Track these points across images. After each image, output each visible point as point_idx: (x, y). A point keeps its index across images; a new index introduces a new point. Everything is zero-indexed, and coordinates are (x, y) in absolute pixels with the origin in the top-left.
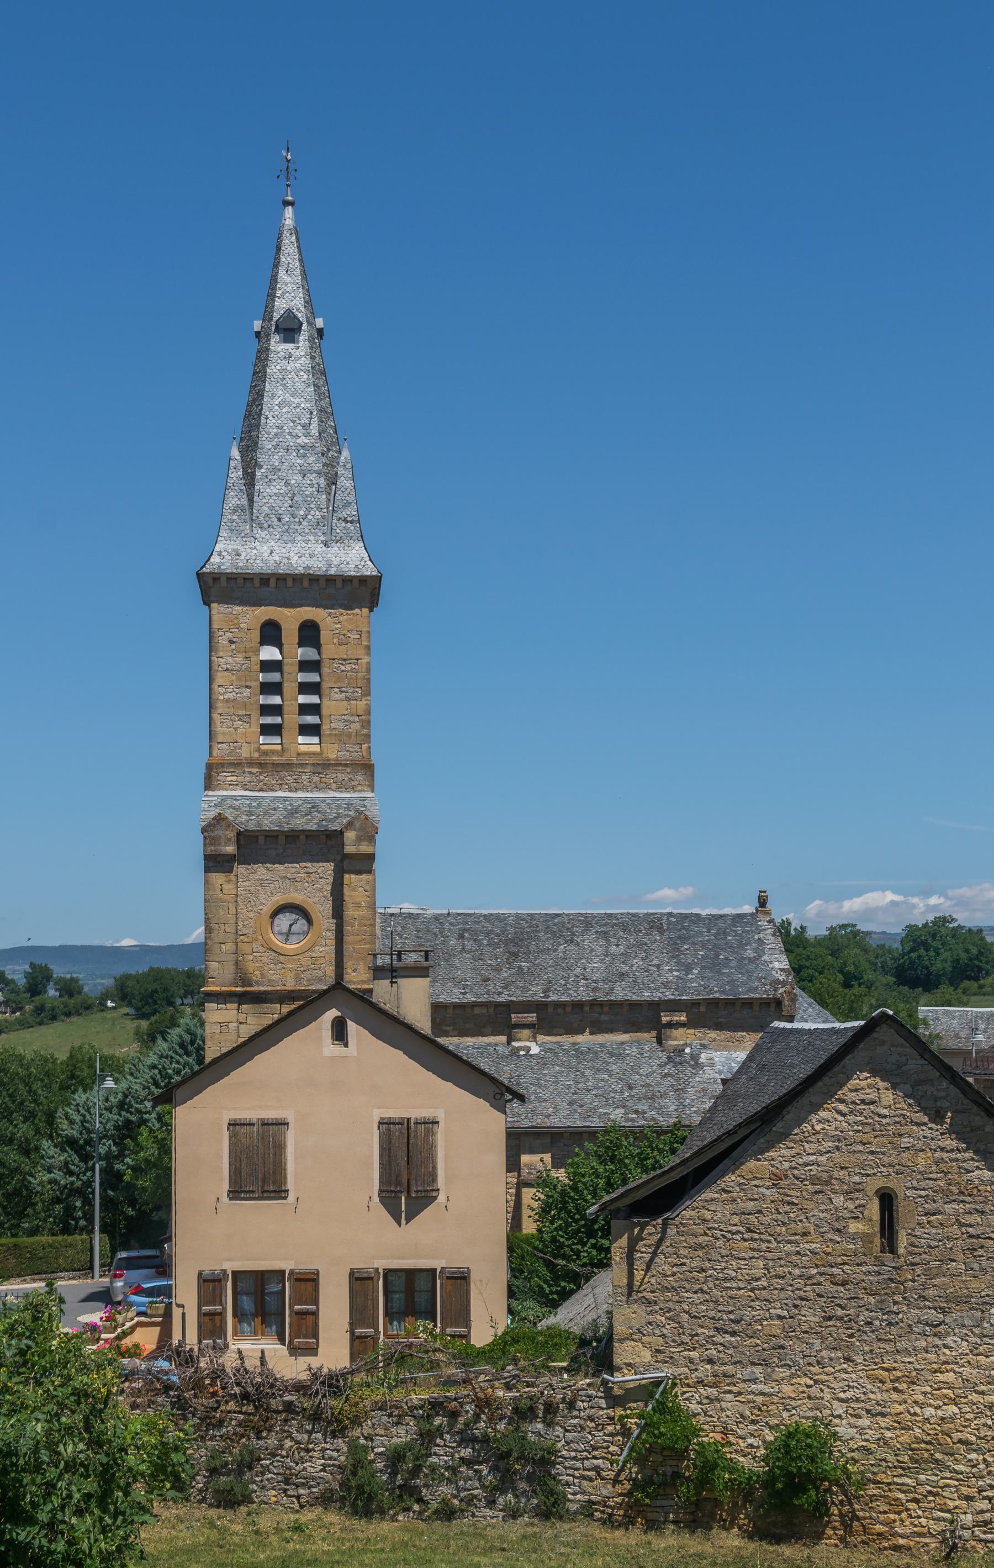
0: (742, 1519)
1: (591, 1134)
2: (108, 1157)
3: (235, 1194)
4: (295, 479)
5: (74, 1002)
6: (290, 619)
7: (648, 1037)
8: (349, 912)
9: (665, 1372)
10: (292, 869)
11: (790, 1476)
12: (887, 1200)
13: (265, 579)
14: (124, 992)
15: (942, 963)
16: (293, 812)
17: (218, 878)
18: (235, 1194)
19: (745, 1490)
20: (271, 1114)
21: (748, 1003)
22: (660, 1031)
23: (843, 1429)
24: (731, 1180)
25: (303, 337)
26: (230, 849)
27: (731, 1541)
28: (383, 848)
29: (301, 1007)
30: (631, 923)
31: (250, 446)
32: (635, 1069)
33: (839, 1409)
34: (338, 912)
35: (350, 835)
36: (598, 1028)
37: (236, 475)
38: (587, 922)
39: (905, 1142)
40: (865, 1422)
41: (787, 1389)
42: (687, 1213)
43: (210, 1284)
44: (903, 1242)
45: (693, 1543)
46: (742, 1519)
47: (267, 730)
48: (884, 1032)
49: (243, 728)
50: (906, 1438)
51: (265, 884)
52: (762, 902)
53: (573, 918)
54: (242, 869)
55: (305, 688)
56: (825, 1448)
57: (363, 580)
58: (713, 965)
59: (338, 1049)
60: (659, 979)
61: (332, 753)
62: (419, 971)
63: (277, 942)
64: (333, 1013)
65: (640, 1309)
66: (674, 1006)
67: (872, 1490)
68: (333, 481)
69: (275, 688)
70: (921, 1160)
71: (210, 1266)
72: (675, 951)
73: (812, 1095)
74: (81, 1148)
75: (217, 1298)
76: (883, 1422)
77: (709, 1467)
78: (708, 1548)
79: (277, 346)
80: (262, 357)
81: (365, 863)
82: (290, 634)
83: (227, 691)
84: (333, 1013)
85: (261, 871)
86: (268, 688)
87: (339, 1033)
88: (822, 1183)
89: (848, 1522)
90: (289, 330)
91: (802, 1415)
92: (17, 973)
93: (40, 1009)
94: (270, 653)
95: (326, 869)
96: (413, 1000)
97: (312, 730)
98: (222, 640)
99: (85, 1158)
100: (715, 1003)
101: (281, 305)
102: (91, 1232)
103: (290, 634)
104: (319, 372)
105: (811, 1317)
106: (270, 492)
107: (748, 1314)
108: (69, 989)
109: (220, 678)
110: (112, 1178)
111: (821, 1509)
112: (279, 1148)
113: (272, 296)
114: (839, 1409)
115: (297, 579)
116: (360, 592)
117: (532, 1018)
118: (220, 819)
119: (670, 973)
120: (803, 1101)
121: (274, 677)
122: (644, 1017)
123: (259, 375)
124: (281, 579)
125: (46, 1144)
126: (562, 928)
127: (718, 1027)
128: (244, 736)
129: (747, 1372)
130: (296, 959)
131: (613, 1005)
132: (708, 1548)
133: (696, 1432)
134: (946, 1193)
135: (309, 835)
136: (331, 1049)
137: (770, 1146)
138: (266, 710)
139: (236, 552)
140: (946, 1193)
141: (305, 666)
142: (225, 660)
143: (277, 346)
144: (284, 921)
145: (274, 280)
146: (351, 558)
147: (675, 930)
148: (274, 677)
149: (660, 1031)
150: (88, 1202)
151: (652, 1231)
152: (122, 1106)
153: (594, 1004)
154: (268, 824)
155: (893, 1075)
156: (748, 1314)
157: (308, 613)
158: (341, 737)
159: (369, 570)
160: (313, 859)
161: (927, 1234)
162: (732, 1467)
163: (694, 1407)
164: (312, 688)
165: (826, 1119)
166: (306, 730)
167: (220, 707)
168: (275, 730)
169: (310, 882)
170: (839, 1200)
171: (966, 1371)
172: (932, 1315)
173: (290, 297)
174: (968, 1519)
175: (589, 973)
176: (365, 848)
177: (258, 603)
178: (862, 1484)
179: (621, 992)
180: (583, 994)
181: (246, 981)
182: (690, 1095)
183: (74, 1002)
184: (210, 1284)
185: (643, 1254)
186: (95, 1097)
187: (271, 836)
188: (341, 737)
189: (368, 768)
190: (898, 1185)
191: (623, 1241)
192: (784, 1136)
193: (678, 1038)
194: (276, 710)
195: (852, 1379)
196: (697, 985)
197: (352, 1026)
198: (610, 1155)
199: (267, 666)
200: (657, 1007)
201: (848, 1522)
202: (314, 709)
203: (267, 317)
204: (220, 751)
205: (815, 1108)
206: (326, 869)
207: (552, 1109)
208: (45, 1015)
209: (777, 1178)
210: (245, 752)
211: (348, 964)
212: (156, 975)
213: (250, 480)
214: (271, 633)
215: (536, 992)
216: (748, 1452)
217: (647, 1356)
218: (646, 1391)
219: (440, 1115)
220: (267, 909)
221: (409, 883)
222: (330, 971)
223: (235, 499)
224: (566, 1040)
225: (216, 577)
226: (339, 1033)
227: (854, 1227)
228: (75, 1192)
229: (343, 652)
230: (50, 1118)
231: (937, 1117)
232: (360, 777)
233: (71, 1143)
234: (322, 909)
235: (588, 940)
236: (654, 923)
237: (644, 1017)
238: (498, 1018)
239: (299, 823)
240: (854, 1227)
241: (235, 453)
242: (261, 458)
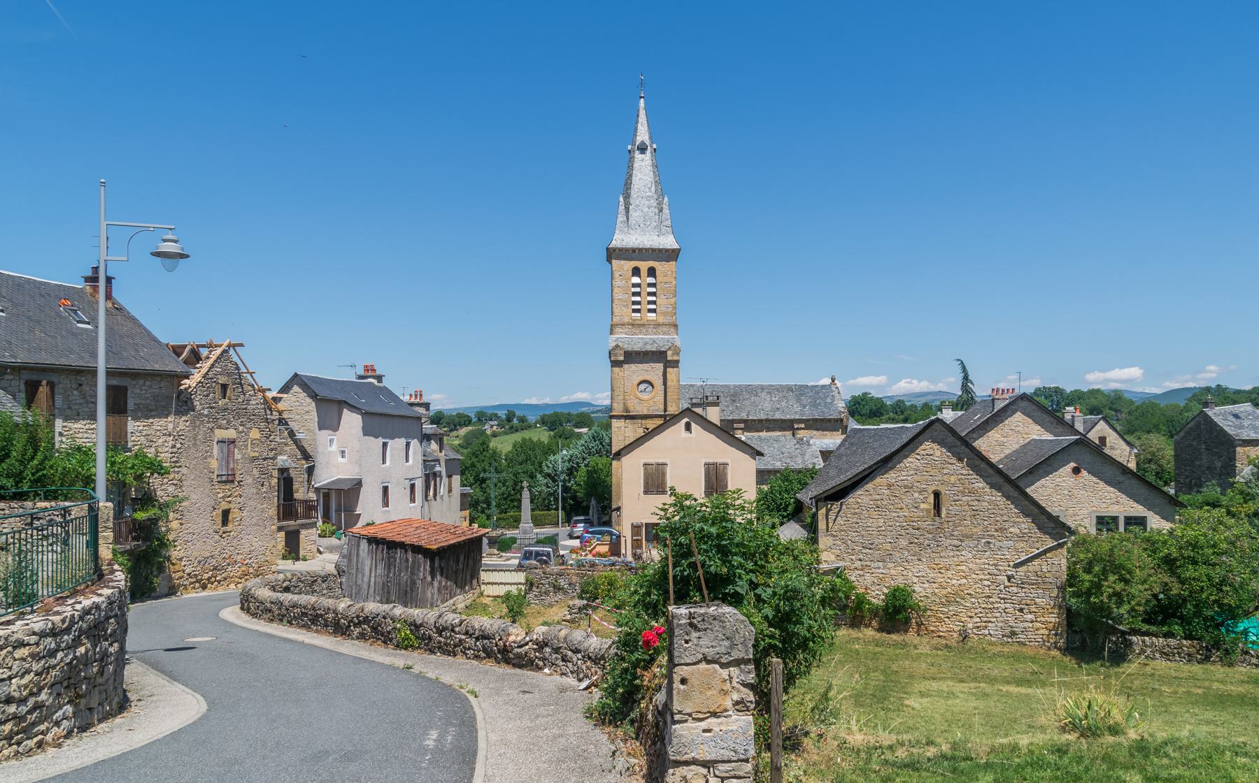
0: (874, 623)
1: (776, 472)
2: (564, 481)
3: (646, 492)
4: (646, 209)
5: (524, 425)
6: (644, 266)
7: (789, 433)
8: (669, 383)
9: (841, 564)
10: (645, 366)
11: (895, 606)
12: (937, 495)
13: (634, 250)
14: (543, 421)
15: (865, 410)
16: (646, 343)
17: (617, 370)
18: (646, 492)
19: (875, 612)
20: (661, 461)
21: (830, 420)
22: (794, 432)
23: (917, 588)
24: (869, 486)
25: (648, 152)
26: (622, 358)
27: (869, 633)
28: (682, 358)
29: (668, 420)
30: (780, 389)
31: (627, 197)
32: (784, 446)
33: (915, 580)
34: (665, 383)
35: (669, 353)
36: (768, 430)
37: (622, 208)
38: (762, 388)
39: (945, 471)
40: (926, 585)
41: (893, 572)
42: (850, 500)
43: (636, 529)
44: (944, 512)
45: (854, 633)
46: (874, 623)
47: (635, 311)
48: (937, 426)
49: (625, 310)
50: (944, 592)
51: (636, 372)
52: (833, 380)
53: (756, 387)
54: (626, 366)
55: (650, 294)
56: (909, 595)
57: (673, 250)
58: (814, 405)
59: (687, 435)
60: (793, 410)
61: (661, 320)
62: (716, 404)
63: (639, 395)
64: (686, 420)
65: (830, 539)
66: (799, 421)
67: (929, 613)
68: (661, 210)
69: (638, 294)
70: (953, 479)
71: (637, 521)
72: (799, 400)
73: (905, 452)
74: (553, 478)
75: (639, 534)
76: (935, 585)
77: (861, 601)
78: (860, 635)
79: (638, 155)
80: (631, 160)
81: (675, 364)
82: (644, 272)
83: (618, 295)
84: (686, 420)
85: (633, 367)
86: (635, 294)
87: (688, 427)
88: (909, 488)
89: (919, 625)
90: (642, 149)
91: (900, 582)
92: (502, 414)
93: (512, 427)
94: (636, 280)
95: (660, 366)
96: (714, 415)
97: (654, 311)
98: (617, 275)
99: (554, 481)
100: (816, 420)
101: (639, 139)
102: (557, 509)
103: (644, 272)
104: (655, 166)
105: (904, 543)
106: (635, 214)
107: (877, 541)
108: (522, 420)
109: (616, 290)
110: (566, 489)
111: (907, 621)
112: (664, 474)
113: (635, 135)
114: (915, 580)
115: (647, 250)
116: (670, 255)
117: (742, 426)
118: (617, 346)
119: (797, 408)
120: (901, 454)
121: (638, 290)
122: (787, 425)
123: (630, 167)
124: (641, 250)
125: (539, 476)
126: (753, 390)
127: (817, 430)
128: (624, 313)
129: (876, 565)
130: (649, 401)
131: (775, 420)
132: (860, 635)
133: (854, 588)
134: (963, 492)
135: (653, 352)
136: (685, 434)
137: (886, 472)
138: (634, 303)
139: (623, 239)
140: (963, 492)
141: (650, 285)
142: (617, 283)
143: (638, 155)
144: (643, 387)
145: (636, 129)
146: (669, 242)
147: (799, 391)
148: (638, 290)
149: (794, 432)
150: (556, 500)
151: (836, 506)
152: (569, 461)
153: (767, 420)
154: (636, 348)
155: (942, 443)
156: (877, 541)
157: (651, 264)
158: (665, 314)
159: (676, 246)
160: (654, 362)
161: (954, 510)
162: (869, 603)
163: (853, 578)
164: (654, 294)
165: (911, 462)
166: (650, 311)
167: (616, 302)
168: (638, 311)
169: (653, 371)
170: (916, 495)
171: (971, 565)
172: (956, 542)
173: (643, 135)
174: (970, 626)
175: (764, 408)
176: (675, 358)
177: (631, 260)
178: (925, 610)
179: (778, 416)
180: (763, 417)
181: (627, 411)
182: (807, 457)
183: (524, 425)
184: (636, 529)
185: (832, 516)
186: (558, 457)
187: (638, 353)
188: (665, 314)
189: (676, 326)
190: (943, 490)
191: (823, 511)
192: (892, 468)
193: (801, 434)
194: (639, 303)
195: (922, 568)
196: (808, 414)
197: (693, 425)
198: (786, 479)
199: (634, 285)
200: (792, 421)
201: (919, 625)
202: (654, 303)
203: (633, 144)
204: (616, 320)
205: (907, 457)
206: (660, 366)
207: (773, 461)
208: (514, 430)
209: (889, 486)
210: (626, 320)
211: (669, 404)
212: (556, 414)
213: (627, 210)
214: (636, 272)
215: (744, 416)
216: (877, 597)
217: (833, 558)
218: (833, 572)
219: (729, 461)
220: (636, 382)
221: (694, 373)
222: (662, 407)
223: (621, 218)
224: (756, 434)
225: (614, 250)
226: (688, 427)
227: (922, 506)
228: (551, 494)
229: (665, 279)
230: (540, 464)
231: (960, 460)
232: (672, 330)
233: (549, 475)
234: (658, 382)
235: (763, 395)
236: (790, 389)
237: (787, 425)
238: (751, 425)
239: (649, 348)
240: (922, 506)
241: (621, 199)
242: (632, 201)
